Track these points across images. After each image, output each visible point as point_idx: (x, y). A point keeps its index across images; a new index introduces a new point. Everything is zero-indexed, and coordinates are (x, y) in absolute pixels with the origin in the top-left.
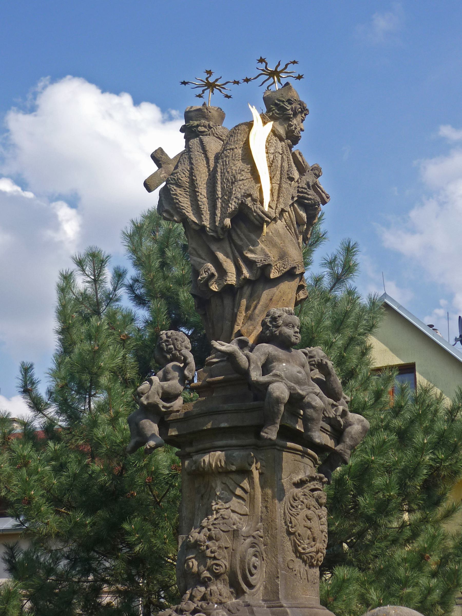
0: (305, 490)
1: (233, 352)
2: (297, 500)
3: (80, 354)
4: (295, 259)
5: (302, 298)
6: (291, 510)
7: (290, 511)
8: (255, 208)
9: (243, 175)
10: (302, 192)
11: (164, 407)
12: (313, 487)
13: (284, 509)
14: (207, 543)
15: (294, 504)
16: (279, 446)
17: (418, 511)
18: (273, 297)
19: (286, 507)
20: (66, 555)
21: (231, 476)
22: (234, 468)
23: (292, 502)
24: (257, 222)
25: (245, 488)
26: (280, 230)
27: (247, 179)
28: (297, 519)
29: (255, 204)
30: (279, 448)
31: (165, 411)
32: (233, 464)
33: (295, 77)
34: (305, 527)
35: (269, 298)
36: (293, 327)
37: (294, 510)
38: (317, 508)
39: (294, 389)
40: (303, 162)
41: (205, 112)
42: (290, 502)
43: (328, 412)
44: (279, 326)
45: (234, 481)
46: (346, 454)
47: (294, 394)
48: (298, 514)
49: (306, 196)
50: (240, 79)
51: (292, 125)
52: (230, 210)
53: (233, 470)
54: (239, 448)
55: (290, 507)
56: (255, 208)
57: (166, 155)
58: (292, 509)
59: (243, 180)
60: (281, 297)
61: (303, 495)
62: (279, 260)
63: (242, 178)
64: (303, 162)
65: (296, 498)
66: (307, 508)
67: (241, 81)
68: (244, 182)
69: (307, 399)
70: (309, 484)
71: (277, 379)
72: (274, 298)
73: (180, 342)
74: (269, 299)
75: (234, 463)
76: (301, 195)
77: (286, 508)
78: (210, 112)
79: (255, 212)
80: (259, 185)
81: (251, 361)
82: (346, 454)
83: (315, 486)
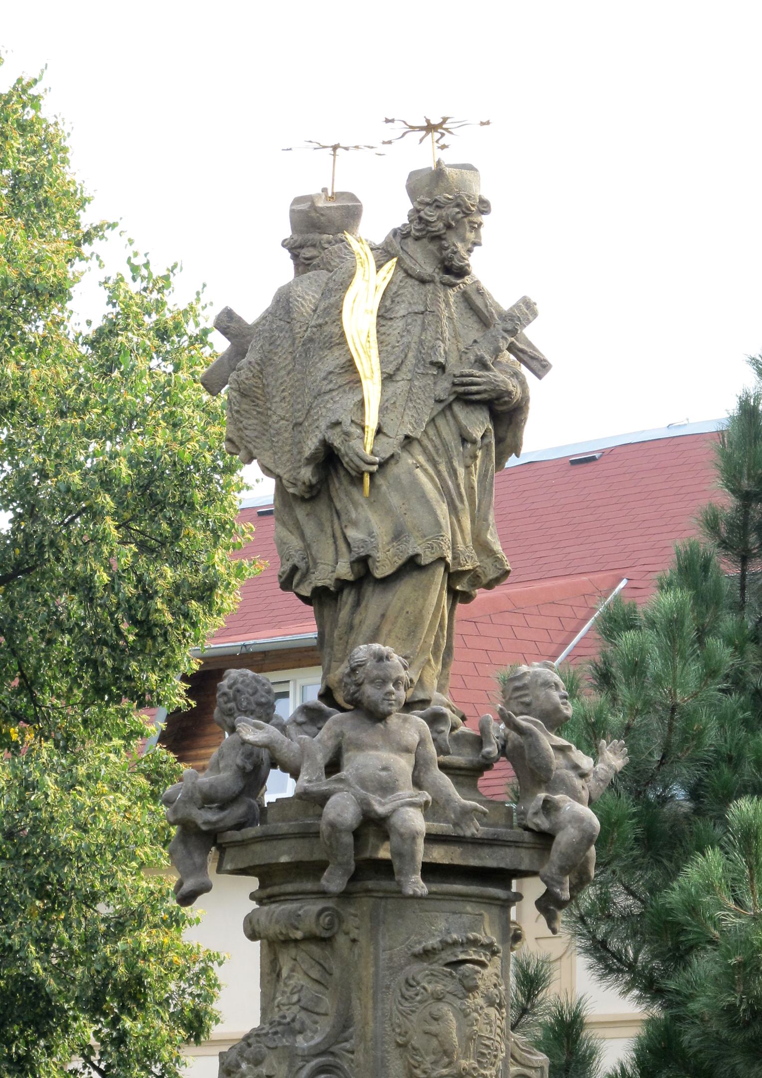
2: (412, 986)
5: (491, 577)
6: (402, 1005)
9: (331, 381)
14: (486, 1011)
17: (551, 1023)
18: (386, 610)
20: (707, 899)
22: (299, 935)
23: (404, 990)
26: (403, 477)
27: (340, 387)
28: (411, 1021)
32: (297, 929)
35: (380, 612)
39: (369, 804)
46: (554, 883)
48: (413, 1011)
49: (474, 388)
50: (377, 143)
51: (447, 249)
52: (307, 453)
53: (298, 937)
54: (314, 896)
57: (240, 320)
58: (403, 1001)
59: (331, 390)
60: (402, 609)
63: (331, 386)
64: (486, 306)
66: (434, 998)
68: (334, 393)
69: (395, 820)
71: (341, 786)
72: (389, 613)
73: (247, 695)
74: (379, 616)
75: (300, 927)
76: (461, 389)
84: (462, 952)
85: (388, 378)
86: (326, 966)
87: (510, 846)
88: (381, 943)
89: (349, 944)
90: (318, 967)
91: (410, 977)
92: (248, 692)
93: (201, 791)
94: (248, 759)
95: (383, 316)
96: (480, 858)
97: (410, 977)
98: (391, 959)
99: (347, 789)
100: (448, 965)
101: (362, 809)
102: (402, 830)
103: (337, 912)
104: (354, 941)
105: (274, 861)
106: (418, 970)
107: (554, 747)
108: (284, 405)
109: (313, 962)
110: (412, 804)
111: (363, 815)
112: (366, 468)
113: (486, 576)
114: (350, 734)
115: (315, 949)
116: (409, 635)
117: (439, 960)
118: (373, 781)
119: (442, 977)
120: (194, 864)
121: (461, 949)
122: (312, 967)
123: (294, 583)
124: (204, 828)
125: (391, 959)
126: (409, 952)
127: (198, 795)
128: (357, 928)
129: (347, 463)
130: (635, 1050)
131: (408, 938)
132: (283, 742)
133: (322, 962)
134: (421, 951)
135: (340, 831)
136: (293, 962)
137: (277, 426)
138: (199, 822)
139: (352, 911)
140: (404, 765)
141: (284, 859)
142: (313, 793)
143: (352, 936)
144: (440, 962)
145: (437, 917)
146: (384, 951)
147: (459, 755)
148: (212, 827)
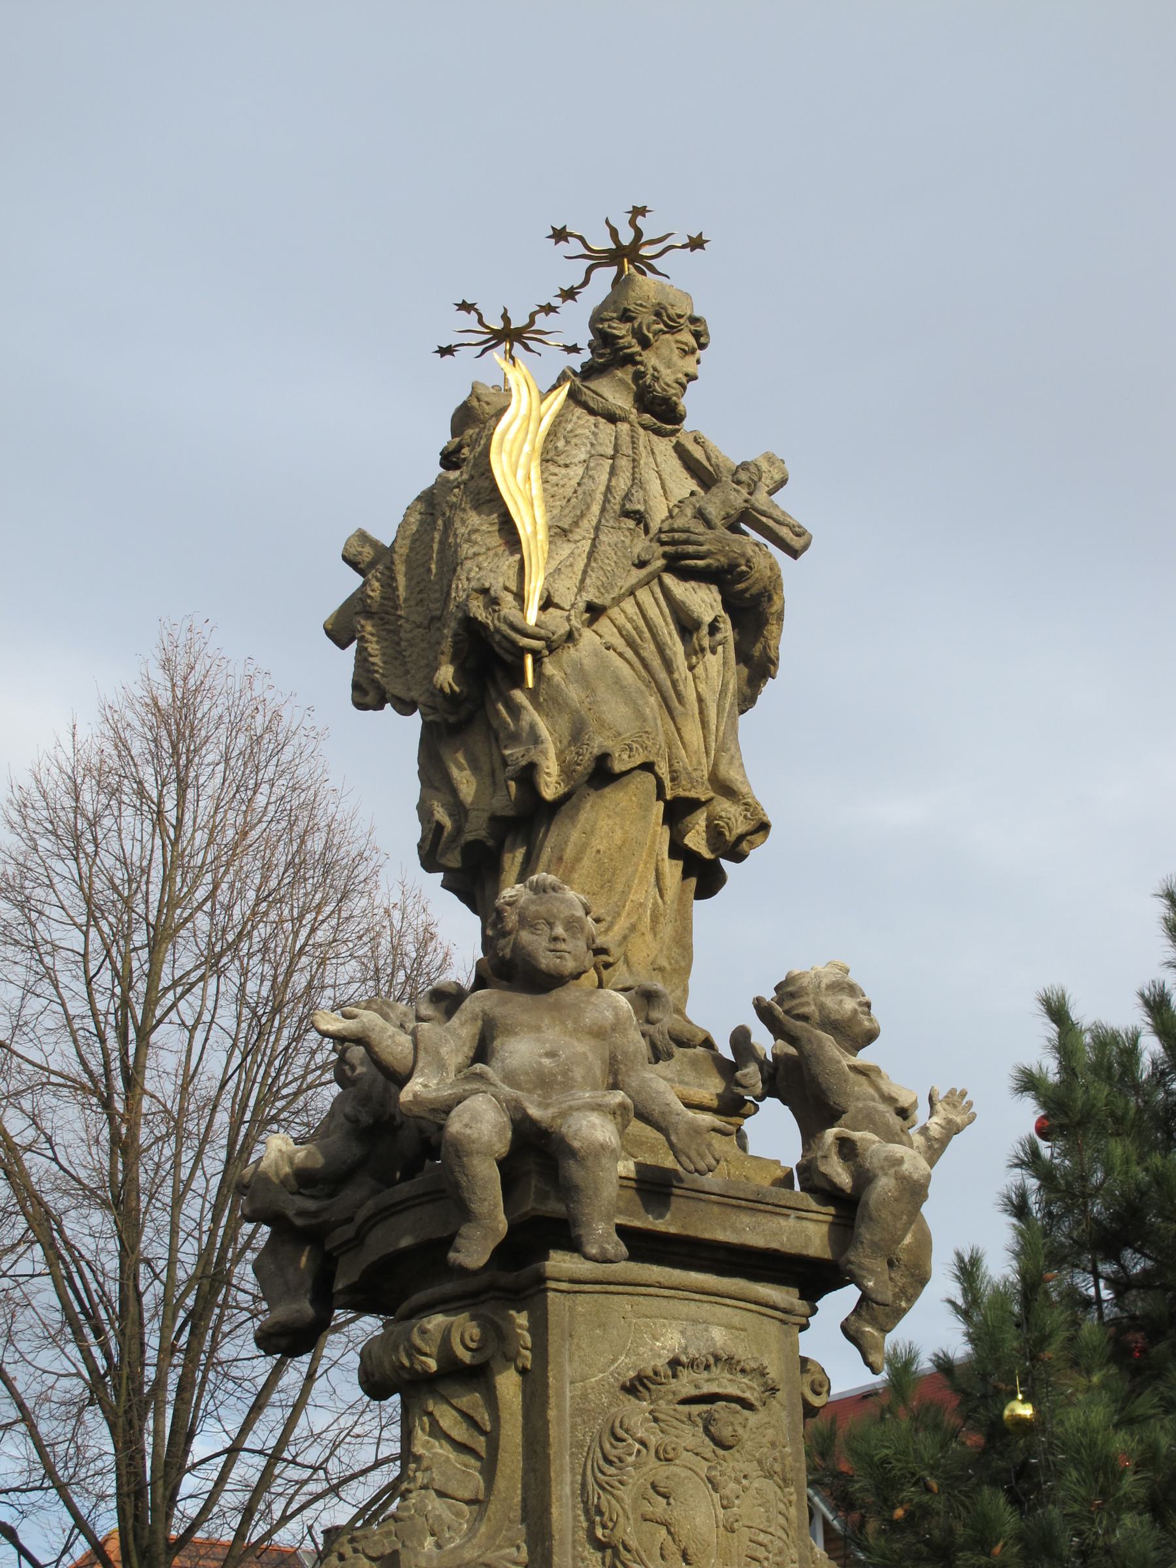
2: (622, 1440)
3: (1154, 1063)
4: (621, 730)
7: (599, 1475)
8: (496, 622)
10: (673, 543)
11: (301, 1213)
12: (690, 1391)
13: (584, 1475)
15: (612, 1453)
19: (589, 1463)
23: (607, 1446)
24: (509, 658)
25: (478, 1418)
26: (586, 661)
29: (495, 611)
30: (564, 1286)
33: (684, 247)
34: (646, 1520)
37: (612, 1470)
38: (709, 1455)
40: (709, 459)
41: (473, 407)
42: (602, 1448)
44: (510, 933)
49: (691, 549)
55: (602, 1462)
56: (496, 622)
62: (570, 745)
64: (709, 459)
65: (620, 1433)
67: (556, 302)
77: (589, 1472)
78: (488, 404)
79: (498, 630)
80: (518, 557)
81: (421, 1046)
84: (708, 1380)
85: (560, 533)
95: (549, 457)
96: (735, 1230)
98: (584, 1396)
99: (484, 1088)
101: (513, 1121)
105: (391, 1249)
106: (636, 1412)
107: (849, 1066)
108: (420, 609)
110: (598, 1108)
112: (525, 642)
113: (730, 830)
114: (498, 1012)
116: (602, 887)
118: (527, 1074)
119: (676, 1423)
121: (705, 1375)
123: (439, 850)
124: (299, 1222)
125: (584, 1396)
129: (499, 643)
130: (1017, 1255)
131: (614, 1361)
132: (383, 1030)
137: (409, 636)
138: (290, 1213)
140: (584, 1053)
141: (406, 1242)
142: (431, 1101)
145: (664, 1326)
146: (572, 1383)
147: (700, 1086)
148: (313, 1221)
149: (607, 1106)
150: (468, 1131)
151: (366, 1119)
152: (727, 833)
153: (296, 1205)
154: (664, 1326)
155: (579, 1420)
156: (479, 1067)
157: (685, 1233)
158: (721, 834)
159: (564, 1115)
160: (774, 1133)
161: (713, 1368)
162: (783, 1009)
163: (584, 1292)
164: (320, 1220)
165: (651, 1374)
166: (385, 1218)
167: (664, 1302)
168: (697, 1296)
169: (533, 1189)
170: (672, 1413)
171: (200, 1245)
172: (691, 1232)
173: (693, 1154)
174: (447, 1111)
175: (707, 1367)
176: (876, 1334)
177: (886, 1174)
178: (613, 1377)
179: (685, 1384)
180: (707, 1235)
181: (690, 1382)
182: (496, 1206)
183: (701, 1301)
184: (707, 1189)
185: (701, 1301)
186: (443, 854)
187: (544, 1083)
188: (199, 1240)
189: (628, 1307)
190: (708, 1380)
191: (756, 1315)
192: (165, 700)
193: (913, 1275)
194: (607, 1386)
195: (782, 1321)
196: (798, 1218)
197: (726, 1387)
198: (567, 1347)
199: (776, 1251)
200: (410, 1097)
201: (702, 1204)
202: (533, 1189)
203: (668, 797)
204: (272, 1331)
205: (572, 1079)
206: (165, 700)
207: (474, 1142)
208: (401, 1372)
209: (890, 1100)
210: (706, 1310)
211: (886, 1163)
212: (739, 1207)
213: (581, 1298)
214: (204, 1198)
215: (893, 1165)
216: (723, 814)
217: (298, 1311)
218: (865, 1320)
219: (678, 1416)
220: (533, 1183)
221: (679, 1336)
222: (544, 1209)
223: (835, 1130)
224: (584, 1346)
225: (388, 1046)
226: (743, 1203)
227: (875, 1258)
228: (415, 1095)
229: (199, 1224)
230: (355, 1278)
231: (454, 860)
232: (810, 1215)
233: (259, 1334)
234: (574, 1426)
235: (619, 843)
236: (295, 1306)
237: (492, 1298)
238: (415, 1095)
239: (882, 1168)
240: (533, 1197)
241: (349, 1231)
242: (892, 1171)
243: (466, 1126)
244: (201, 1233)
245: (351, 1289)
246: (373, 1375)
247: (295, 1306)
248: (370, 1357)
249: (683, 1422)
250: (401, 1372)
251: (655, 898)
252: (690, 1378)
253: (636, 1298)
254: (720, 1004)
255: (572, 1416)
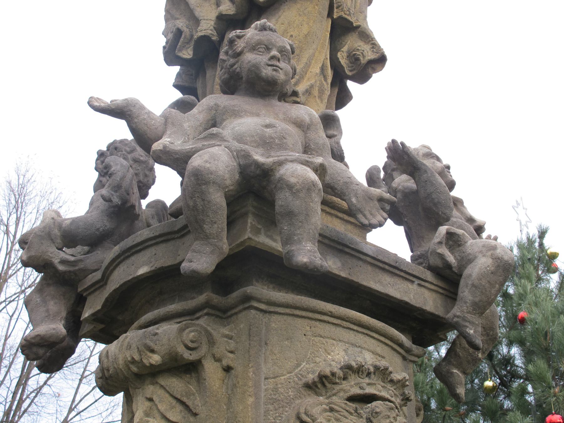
0: (335, 399)
1: (125, 107)
11: (63, 262)
12: (356, 391)
16: (259, 301)
21: (162, 381)
22: (155, 359)
30: (263, 306)
31: (65, 272)
32: (153, 351)
36: (268, 49)
39: (247, 156)
43: (369, 216)
45: (168, 392)
46: (467, 324)
47: (249, 165)
61: (325, 410)
70: (345, 385)
75: (156, 348)
82: (467, 324)
83: (361, 388)
84: (369, 384)
86: (189, 403)
87: (413, 282)
88: (264, 369)
89: (220, 374)
90: (179, 407)
91: (302, 410)
92: (125, 150)
93: (60, 226)
94: (116, 191)
97: (302, 410)
98: (275, 390)
100: (353, 399)
101: (240, 165)
102: (293, 180)
103: (207, 331)
104: (228, 369)
109: (174, 402)
111: (241, 173)
113: (364, 57)
115: (175, 384)
117: (339, 392)
118: (253, 136)
119: (346, 414)
120: (47, 311)
121: (367, 380)
122: (173, 407)
124: (61, 268)
125: (275, 390)
126: (300, 383)
127: (56, 232)
128: (232, 352)
131: (298, 365)
133: (185, 399)
134: (316, 379)
135: (207, 183)
136: (148, 404)
138: (56, 261)
139: (226, 331)
141: (142, 271)
142: (176, 153)
143: (225, 363)
144: (342, 394)
145: (333, 345)
146: (266, 378)
148: (72, 269)
149: (312, 163)
150: (208, 165)
151: (116, 200)
152: (361, 58)
153: (59, 256)
154: (333, 345)
155: (271, 407)
156: (214, 130)
157: (350, 278)
158: (357, 59)
159: (281, 163)
160: (390, 239)
161: (373, 376)
162: (400, 157)
163: (280, 314)
164: (77, 268)
165: (329, 374)
166: (129, 257)
167: (333, 328)
168: (355, 328)
169: (249, 225)
170: (343, 405)
171: (5, 408)
172: (355, 279)
173: (367, 213)
174: (189, 157)
175: (369, 374)
176: (460, 375)
177: (484, 256)
178: (297, 377)
179: (353, 387)
180: (365, 283)
181: (356, 384)
182: (222, 229)
183: (357, 331)
184: (365, 251)
185: (357, 331)
186: (180, 50)
187: (266, 143)
188: (5, 406)
189: (308, 328)
190: (369, 384)
191: (390, 349)
192: (14, 183)
193: (488, 335)
194: (293, 384)
195: (404, 358)
196: (419, 285)
197: (380, 392)
198: (263, 351)
199: (407, 303)
200: (161, 147)
201: (360, 263)
202: (249, 225)
203: (335, 17)
204: (33, 341)
205: (286, 143)
206: (14, 183)
207: (211, 174)
208: (131, 366)
209: (471, 220)
210: (360, 339)
211: (484, 249)
212: (383, 269)
213: (275, 317)
214: (9, 388)
215: (490, 250)
216: (359, 48)
217: (54, 329)
218: (453, 365)
219: (348, 409)
220: (249, 221)
221: (343, 353)
222: (257, 239)
223: (446, 227)
224: (276, 352)
225: (144, 119)
226: (387, 267)
227: (475, 314)
228: (165, 147)
229: (6, 399)
230: (99, 307)
231: (187, 54)
232: (427, 284)
233: (24, 342)
234: (267, 412)
235: (306, 33)
236: (53, 326)
237: (207, 314)
238: (165, 147)
239: (481, 252)
240: (249, 230)
241: (98, 276)
242: (489, 253)
243: (206, 162)
244: (6, 402)
245: (95, 317)
246: (108, 370)
247: (53, 326)
248: (107, 356)
249: (351, 414)
250: (131, 366)
251: (320, 81)
252: (356, 382)
253: (313, 322)
254: (362, 152)
255: (265, 404)
